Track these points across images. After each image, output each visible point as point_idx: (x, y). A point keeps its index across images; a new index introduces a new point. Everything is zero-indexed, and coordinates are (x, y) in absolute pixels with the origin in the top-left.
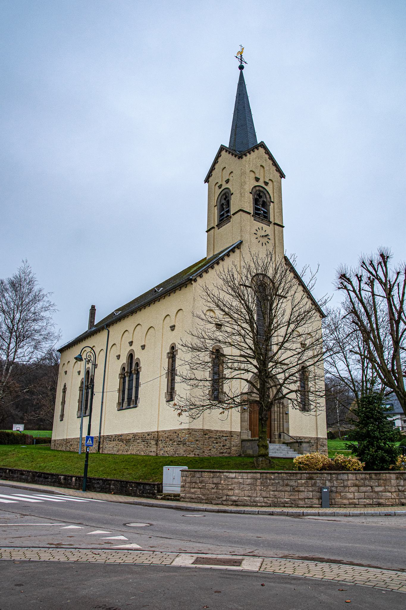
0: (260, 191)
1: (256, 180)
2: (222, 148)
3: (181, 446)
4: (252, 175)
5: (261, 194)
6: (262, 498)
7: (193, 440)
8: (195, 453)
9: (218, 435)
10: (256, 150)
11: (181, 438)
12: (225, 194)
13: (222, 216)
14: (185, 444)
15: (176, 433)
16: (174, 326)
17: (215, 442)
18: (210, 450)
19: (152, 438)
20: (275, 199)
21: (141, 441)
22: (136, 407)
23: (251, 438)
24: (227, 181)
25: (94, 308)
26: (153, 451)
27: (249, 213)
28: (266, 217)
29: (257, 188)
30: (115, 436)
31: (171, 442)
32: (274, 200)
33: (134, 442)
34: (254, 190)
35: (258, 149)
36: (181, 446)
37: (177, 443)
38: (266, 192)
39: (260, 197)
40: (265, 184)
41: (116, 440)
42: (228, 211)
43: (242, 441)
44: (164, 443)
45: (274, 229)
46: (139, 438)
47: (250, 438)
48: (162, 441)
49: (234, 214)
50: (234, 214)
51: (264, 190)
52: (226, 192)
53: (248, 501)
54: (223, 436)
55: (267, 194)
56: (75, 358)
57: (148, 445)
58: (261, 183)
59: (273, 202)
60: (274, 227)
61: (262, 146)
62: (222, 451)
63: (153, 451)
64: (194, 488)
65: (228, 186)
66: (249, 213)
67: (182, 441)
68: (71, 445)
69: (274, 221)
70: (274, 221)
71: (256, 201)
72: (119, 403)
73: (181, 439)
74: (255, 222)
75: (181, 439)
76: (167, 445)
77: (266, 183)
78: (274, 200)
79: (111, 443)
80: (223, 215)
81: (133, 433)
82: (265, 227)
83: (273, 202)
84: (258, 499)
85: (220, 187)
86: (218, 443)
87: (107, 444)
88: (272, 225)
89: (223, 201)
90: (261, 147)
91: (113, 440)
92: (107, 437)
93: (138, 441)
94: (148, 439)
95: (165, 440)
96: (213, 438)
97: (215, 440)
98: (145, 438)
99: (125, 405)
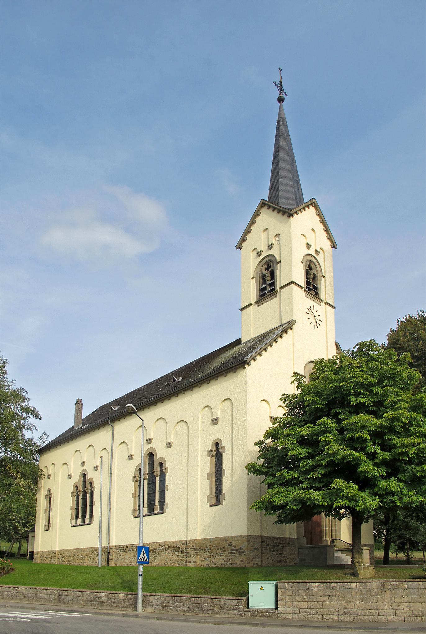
0: (311, 261)
1: (307, 246)
2: (263, 203)
3: (237, 555)
4: (304, 241)
5: (312, 266)
6: (393, 611)
7: (252, 547)
8: (254, 562)
9: (274, 542)
10: (307, 209)
11: (236, 546)
12: (267, 263)
13: (262, 290)
14: (243, 552)
15: (226, 541)
16: (217, 419)
17: (272, 550)
18: (268, 558)
19: (191, 547)
20: (326, 274)
21: (173, 550)
22: (162, 513)
23: (307, 545)
24: (270, 247)
25: (81, 401)
26: (192, 561)
27: (302, 287)
28: (317, 294)
29: (309, 257)
30: (132, 546)
31: (220, 551)
32: (325, 274)
33: (161, 552)
34: (305, 259)
35: (309, 208)
36: (237, 555)
37: (230, 552)
38: (317, 264)
39: (311, 269)
40: (316, 253)
41: (133, 550)
42: (273, 284)
43: (298, 549)
44: (209, 552)
45: (326, 310)
46: (170, 547)
47: (306, 545)
48: (205, 550)
49: (282, 288)
50: (282, 288)
51: (315, 261)
52: (269, 260)
53: (375, 614)
54: (279, 543)
55: (318, 267)
56: (225, 446)
57: (186, 555)
58: (312, 251)
59: (324, 277)
60: (326, 307)
61: (314, 205)
62: (279, 559)
63: (192, 561)
64: (299, 601)
65: (270, 252)
66: (302, 287)
67: (237, 550)
68: (64, 557)
69: (326, 299)
70: (326, 299)
71: (307, 273)
72: (134, 510)
73: (235, 547)
74: (306, 298)
75: (235, 547)
76: (214, 554)
77: (317, 252)
78: (325, 274)
79: (126, 554)
80: (265, 289)
81: (159, 543)
82: (317, 306)
83: (324, 277)
84: (387, 611)
85: (259, 254)
86: (275, 551)
87: (120, 555)
88: (323, 304)
89: (265, 272)
90: (313, 206)
91: (129, 551)
92: (120, 548)
93: (169, 551)
94: (183, 549)
95: (210, 549)
96: (270, 545)
97: (272, 548)
98: (179, 547)
99: (145, 510)
